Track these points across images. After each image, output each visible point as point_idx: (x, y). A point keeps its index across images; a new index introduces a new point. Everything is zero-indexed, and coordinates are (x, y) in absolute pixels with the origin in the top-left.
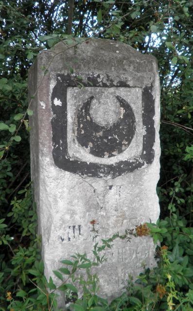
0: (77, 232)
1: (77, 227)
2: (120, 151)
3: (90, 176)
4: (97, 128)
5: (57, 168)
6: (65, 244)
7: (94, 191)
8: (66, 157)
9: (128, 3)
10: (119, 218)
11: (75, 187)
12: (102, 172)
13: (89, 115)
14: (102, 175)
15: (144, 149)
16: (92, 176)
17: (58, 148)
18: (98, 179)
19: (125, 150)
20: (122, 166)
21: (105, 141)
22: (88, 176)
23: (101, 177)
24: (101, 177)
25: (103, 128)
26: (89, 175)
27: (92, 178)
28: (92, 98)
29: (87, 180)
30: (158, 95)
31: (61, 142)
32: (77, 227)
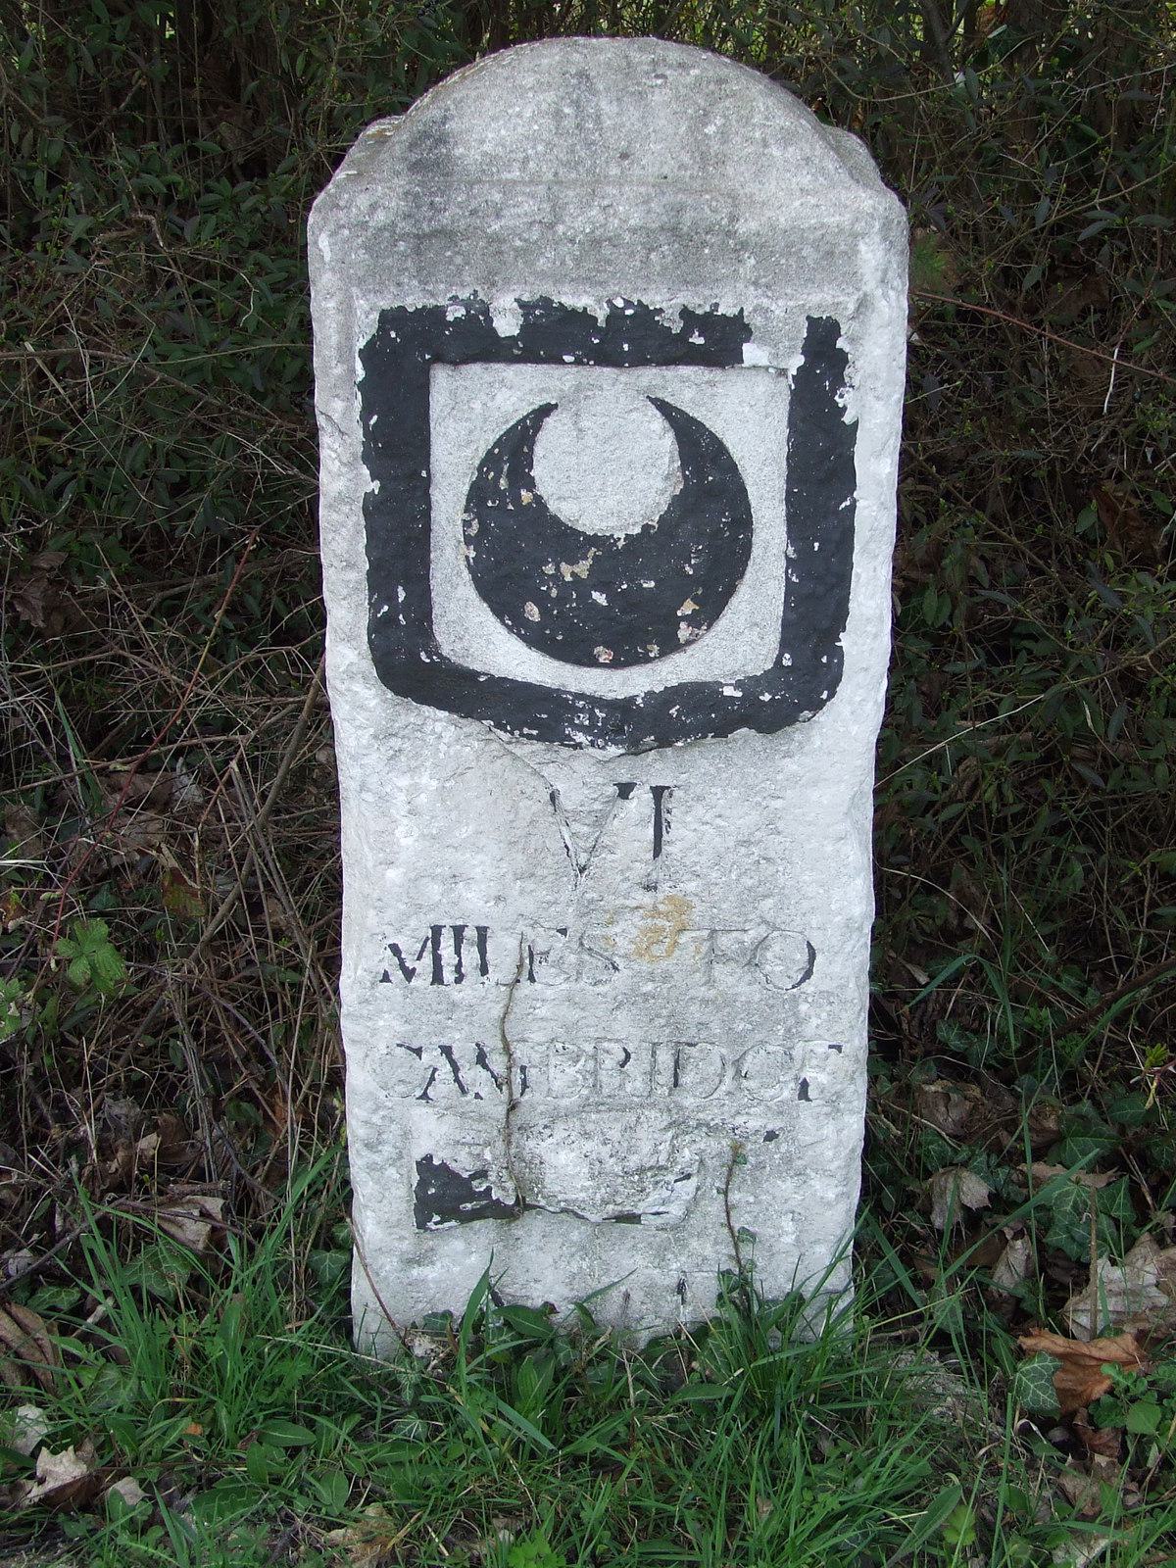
0: (470, 956)
1: (470, 933)
2: (671, 646)
3: (530, 737)
4: (568, 541)
5: (390, 695)
6: (415, 989)
7: (553, 797)
8: (423, 656)
9: (1167, 138)
10: (660, 922)
11: (469, 774)
12: (581, 728)
13: (531, 485)
14: (580, 737)
15: (785, 645)
16: (538, 738)
17: (390, 620)
18: (565, 752)
19: (689, 643)
20: (673, 711)
21: (600, 598)
22: (522, 735)
23: (578, 746)
24: (578, 746)
25: (595, 540)
26: (526, 731)
27: (538, 746)
28: (546, 410)
29: (518, 750)
30: (349, 639)
31: (402, 595)
32: (470, 933)
